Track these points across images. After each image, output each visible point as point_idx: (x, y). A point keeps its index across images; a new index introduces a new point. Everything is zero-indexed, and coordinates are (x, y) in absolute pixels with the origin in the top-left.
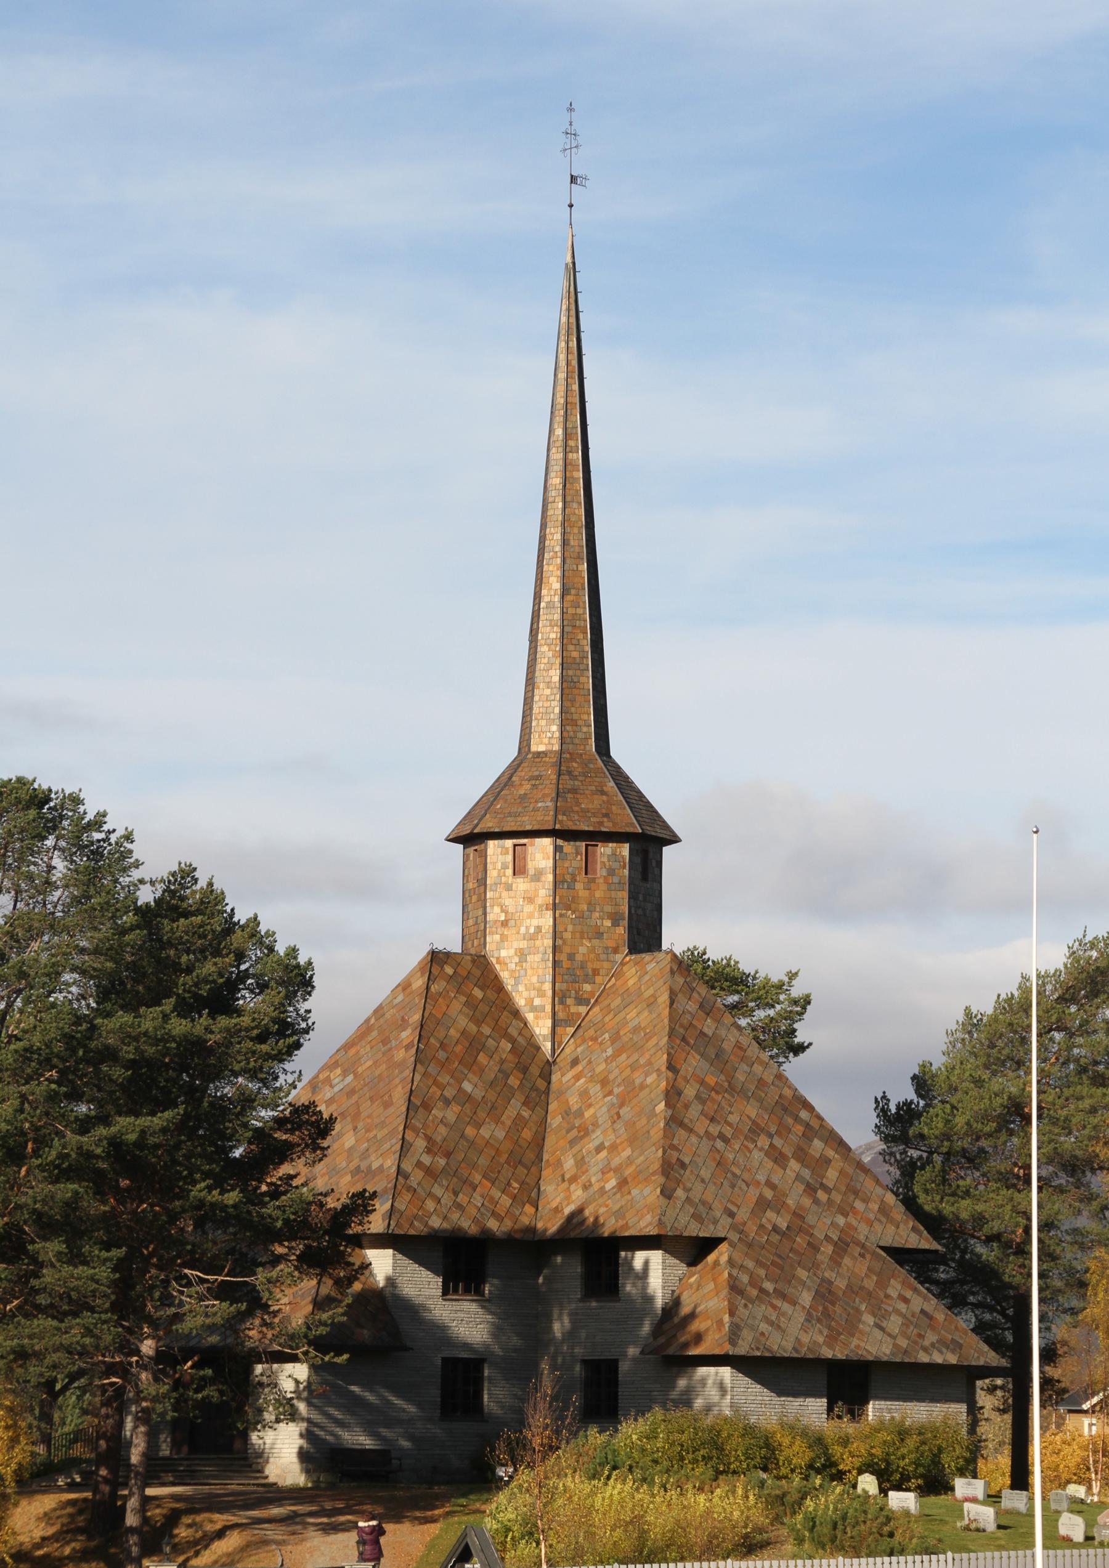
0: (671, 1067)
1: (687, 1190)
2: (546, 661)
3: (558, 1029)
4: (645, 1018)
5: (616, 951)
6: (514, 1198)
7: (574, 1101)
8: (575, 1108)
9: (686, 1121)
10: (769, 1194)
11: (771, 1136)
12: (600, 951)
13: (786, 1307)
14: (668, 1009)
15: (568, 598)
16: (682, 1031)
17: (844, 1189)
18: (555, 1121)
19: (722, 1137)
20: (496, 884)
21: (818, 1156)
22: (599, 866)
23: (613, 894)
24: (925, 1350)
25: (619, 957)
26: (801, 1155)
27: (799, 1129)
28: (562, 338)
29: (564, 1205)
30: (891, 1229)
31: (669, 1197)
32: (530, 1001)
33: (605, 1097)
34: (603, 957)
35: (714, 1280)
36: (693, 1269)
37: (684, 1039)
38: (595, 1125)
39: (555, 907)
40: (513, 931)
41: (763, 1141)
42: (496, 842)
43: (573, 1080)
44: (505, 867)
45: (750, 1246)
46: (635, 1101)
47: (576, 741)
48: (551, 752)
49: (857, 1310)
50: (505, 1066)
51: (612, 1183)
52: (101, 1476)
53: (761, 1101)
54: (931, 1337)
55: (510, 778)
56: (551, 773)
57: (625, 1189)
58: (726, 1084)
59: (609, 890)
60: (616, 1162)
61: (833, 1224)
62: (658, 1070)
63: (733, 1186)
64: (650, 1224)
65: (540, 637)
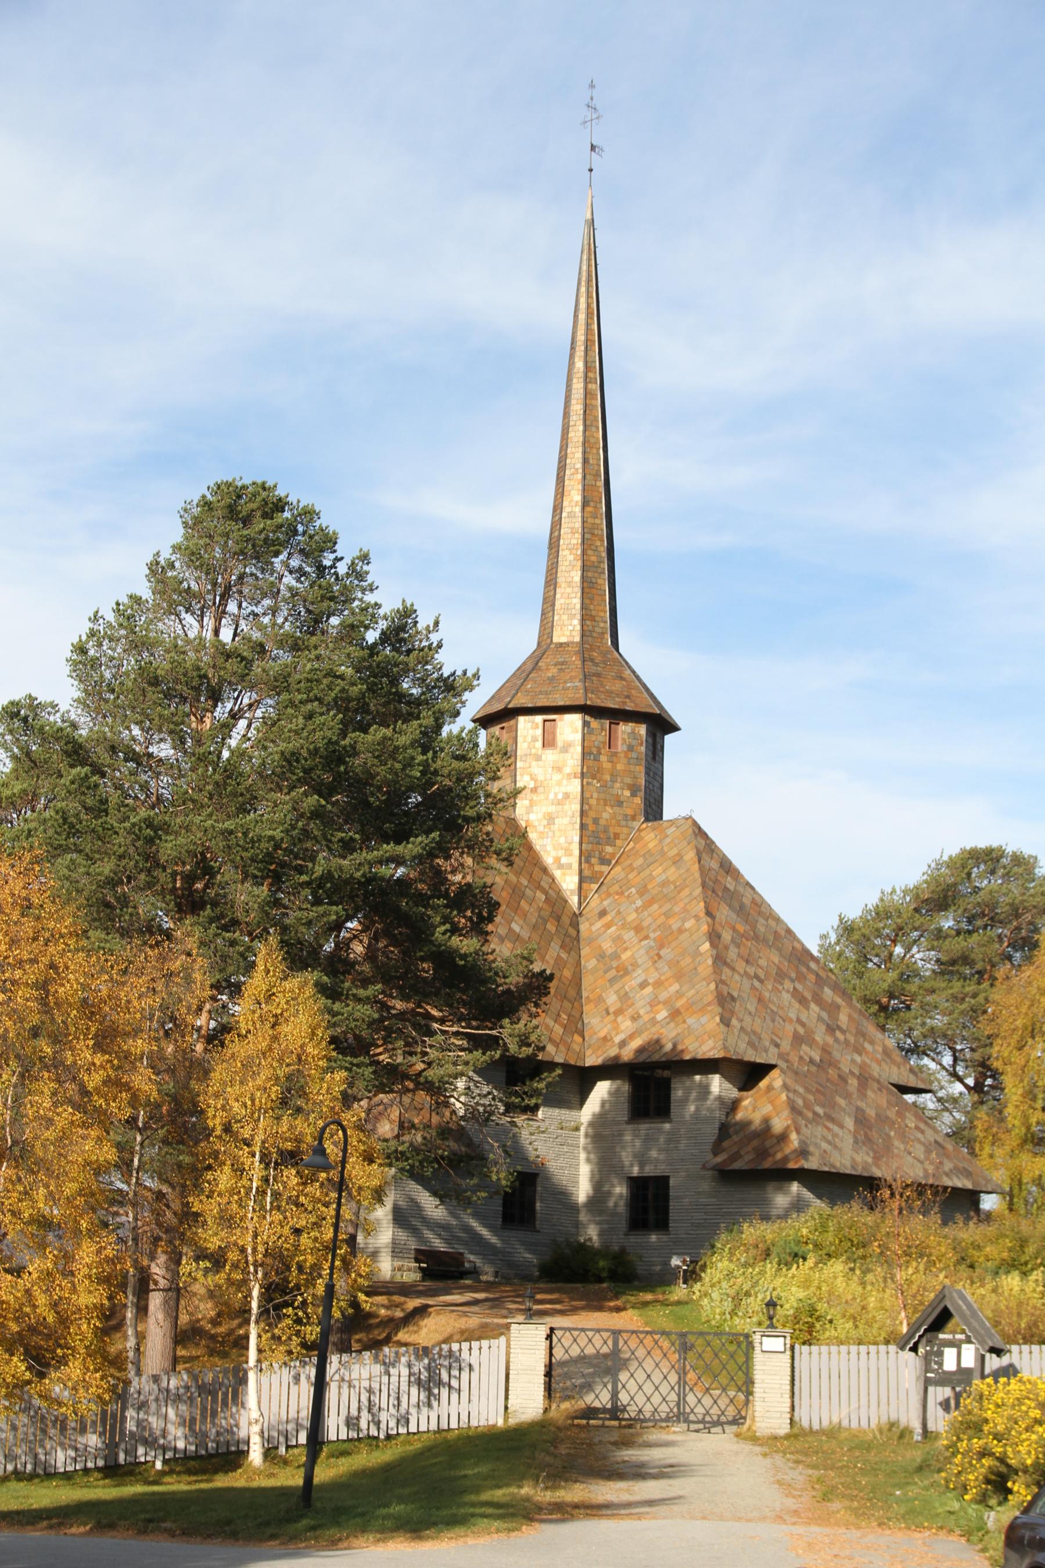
0: (709, 913)
1: (741, 1021)
2: (567, 563)
3: (584, 885)
4: (672, 873)
5: (634, 818)
6: (565, 1027)
7: (607, 946)
8: (610, 951)
9: (728, 960)
10: (801, 1031)
11: (793, 981)
12: (620, 818)
13: (836, 1129)
14: (697, 865)
15: (588, 509)
16: (711, 883)
17: (854, 1032)
18: (589, 964)
19: (757, 977)
20: (526, 755)
21: (830, 1001)
22: (620, 742)
23: (632, 768)
24: (947, 1175)
25: (636, 824)
26: (818, 1000)
27: (812, 977)
28: (583, 284)
29: (613, 1033)
30: (895, 1069)
31: (728, 1025)
32: (557, 860)
33: (641, 941)
34: (623, 823)
35: (771, 1102)
36: (745, 1093)
37: (713, 891)
38: (635, 965)
39: (583, 775)
40: (542, 797)
41: (788, 985)
42: (527, 718)
43: (603, 929)
44: (534, 739)
45: (796, 1073)
46: (674, 944)
47: (595, 635)
48: (573, 643)
49: (888, 1136)
50: (542, 913)
51: (662, 1014)
52: (989, 1086)
53: (780, 950)
54: (948, 1166)
55: (537, 664)
56: (576, 660)
57: (679, 1019)
58: (752, 933)
59: (629, 763)
60: (664, 996)
61: (853, 1061)
62: (696, 916)
63: (773, 1021)
64: (714, 1048)
65: (562, 542)
